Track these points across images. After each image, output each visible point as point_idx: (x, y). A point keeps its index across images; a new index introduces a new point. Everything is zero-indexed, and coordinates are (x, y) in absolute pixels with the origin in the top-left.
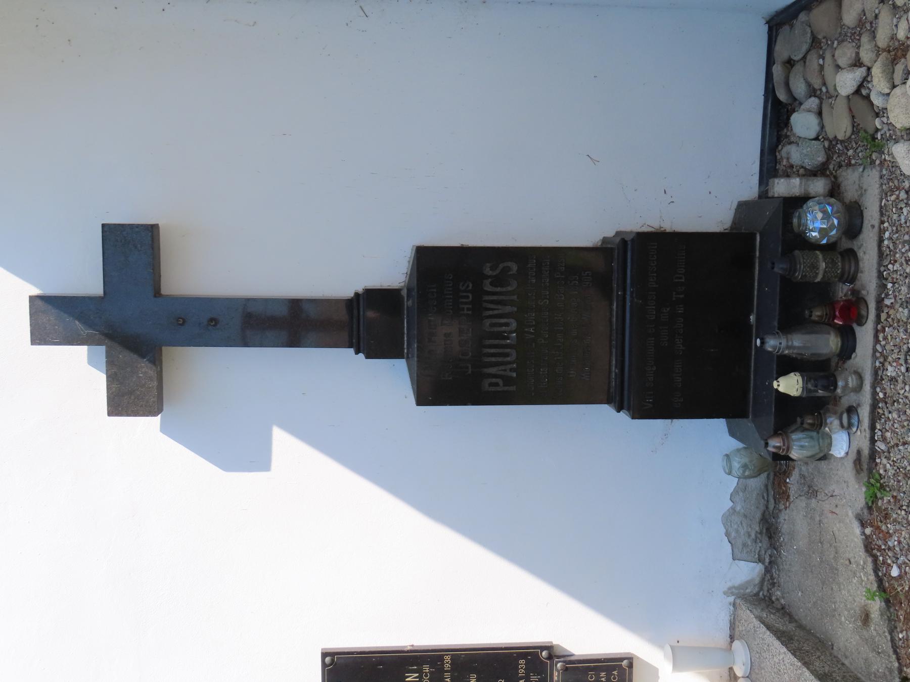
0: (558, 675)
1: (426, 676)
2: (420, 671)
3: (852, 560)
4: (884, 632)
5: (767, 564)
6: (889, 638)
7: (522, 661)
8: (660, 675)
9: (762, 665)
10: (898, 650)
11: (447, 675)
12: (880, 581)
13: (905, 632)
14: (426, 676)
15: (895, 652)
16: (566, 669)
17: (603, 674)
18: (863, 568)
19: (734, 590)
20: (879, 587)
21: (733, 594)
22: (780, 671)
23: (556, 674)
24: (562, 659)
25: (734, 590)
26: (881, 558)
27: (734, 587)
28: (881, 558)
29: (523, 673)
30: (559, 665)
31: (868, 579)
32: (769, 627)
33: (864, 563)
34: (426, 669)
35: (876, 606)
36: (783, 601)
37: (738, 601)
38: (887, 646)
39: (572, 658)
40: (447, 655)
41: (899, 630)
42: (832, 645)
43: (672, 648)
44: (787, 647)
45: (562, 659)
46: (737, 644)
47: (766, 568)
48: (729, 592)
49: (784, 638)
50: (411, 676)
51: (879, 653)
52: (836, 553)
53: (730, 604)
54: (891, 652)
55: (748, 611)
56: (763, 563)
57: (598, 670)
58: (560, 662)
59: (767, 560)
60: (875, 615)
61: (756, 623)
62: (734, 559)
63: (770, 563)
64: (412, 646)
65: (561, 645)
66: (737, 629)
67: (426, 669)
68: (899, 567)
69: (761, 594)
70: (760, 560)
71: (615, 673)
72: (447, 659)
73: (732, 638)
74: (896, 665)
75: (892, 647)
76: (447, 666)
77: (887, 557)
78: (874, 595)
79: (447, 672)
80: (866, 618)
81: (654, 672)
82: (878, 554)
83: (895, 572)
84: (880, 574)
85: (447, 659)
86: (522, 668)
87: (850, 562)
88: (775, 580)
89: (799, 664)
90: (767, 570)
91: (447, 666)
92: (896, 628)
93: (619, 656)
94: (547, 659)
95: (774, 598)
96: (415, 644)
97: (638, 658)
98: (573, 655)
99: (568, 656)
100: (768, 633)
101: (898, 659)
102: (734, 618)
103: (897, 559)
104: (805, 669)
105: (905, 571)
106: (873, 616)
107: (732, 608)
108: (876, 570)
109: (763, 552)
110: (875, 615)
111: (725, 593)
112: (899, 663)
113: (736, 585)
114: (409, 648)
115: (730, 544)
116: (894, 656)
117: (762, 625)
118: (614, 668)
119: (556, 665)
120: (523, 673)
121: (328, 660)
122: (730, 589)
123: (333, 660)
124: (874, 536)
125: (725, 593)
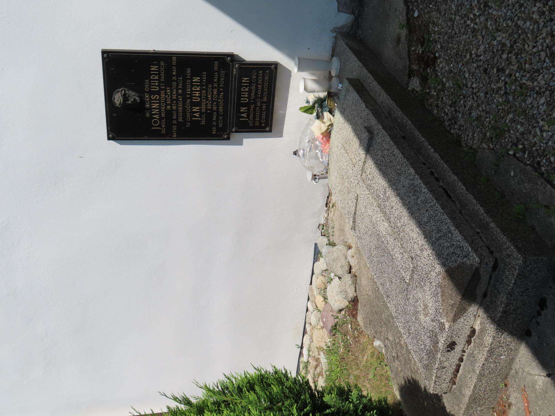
0: (236, 71)
1: (162, 68)
2: (158, 64)
3: (397, 9)
4: (406, 47)
5: (356, 15)
6: (407, 50)
7: (216, 62)
8: (292, 74)
9: (345, 69)
10: (410, 56)
11: (174, 73)
12: (408, 19)
13: (415, 47)
14: (162, 68)
15: (409, 57)
16: (240, 68)
17: (261, 72)
18: (402, 13)
19: (336, 30)
20: (407, 23)
21: (335, 31)
22: (352, 70)
23: (235, 70)
24: (238, 63)
25: (336, 30)
26: (411, 7)
27: (337, 28)
28: (411, 7)
29: (217, 69)
30: (237, 65)
31: (403, 19)
32: (350, 48)
33: (403, 10)
34: (162, 63)
35: (404, 32)
36: (362, 37)
37: (338, 35)
38: (405, 55)
39: (245, 62)
40: (174, 56)
41: (413, 46)
42: (381, 57)
43: (299, 59)
44: (358, 58)
45: (238, 63)
46: (334, 59)
47: (356, 18)
48: (333, 31)
49: (357, 53)
50: (154, 67)
51: (401, 58)
52: (390, 6)
53: (334, 37)
54: (407, 57)
55: (342, 41)
56: (354, 15)
57: (258, 69)
58: (237, 64)
59: (357, 13)
60: (403, 38)
61: (345, 46)
62: (339, 11)
63: (358, 15)
64: (154, 50)
65: (238, 55)
66: (336, 52)
67: (162, 63)
68: (419, 11)
69: (351, 32)
70: (353, 13)
71: (267, 71)
72: (174, 59)
73: (332, 56)
74: (408, 63)
75: (408, 55)
76: (174, 63)
77: (414, 6)
78: (403, 26)
79: (174, 66)
80: (398, 40)
81: (289, 73)
82: (410, 5)
83: (416, 15)
84: (409, 16)
85: (174, 59)
86: (216, 66)
87: (396, 11)
88: (359, 25)
89: (362, 66)
90: (356, 19)
91: (174, 63)
92: (412, 45)
93: (270, 63)
94: (230, 61)
95: (357, 35)
96: (156, 50)
97: (281, 65)
98: (245, 61)
99: (242, 61)
100: (350, 51)
101: (410, 61)
102: (335, 46)
103: (419, 7)
104: (364, 68)
105: (421, 14)
106: (402, 39)
107: (334, 40)
108: (407, 14)
109: (355, 9)
110: (403, 38)
111: (331, 31)
112: (410, 63)
113: (338, 27)
114: (152, 51)
115: (337, 3)
116: (408, 59)
117: (348, 47)
118: (267, 69)
119: (235, 66)
120: (217, 69)
121: (105, 55)
122: (334, 28)
123: (108, 56)
124: (467, 76)
125: (331, 31)
